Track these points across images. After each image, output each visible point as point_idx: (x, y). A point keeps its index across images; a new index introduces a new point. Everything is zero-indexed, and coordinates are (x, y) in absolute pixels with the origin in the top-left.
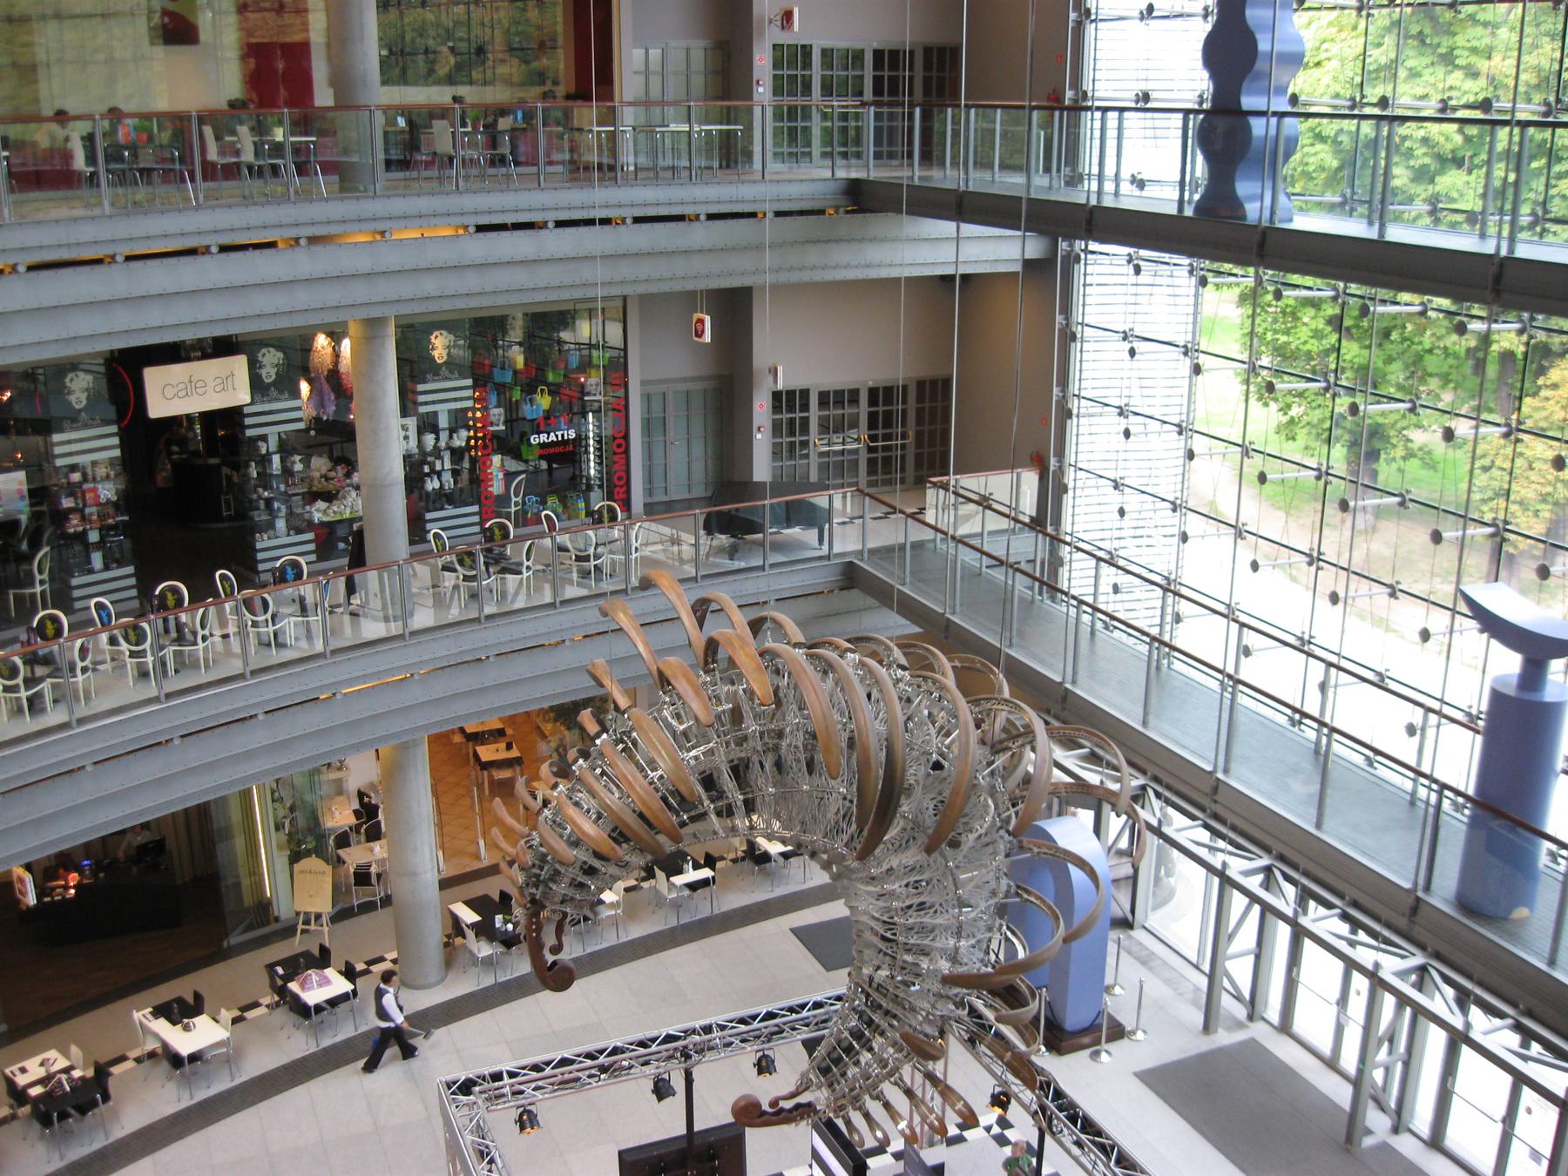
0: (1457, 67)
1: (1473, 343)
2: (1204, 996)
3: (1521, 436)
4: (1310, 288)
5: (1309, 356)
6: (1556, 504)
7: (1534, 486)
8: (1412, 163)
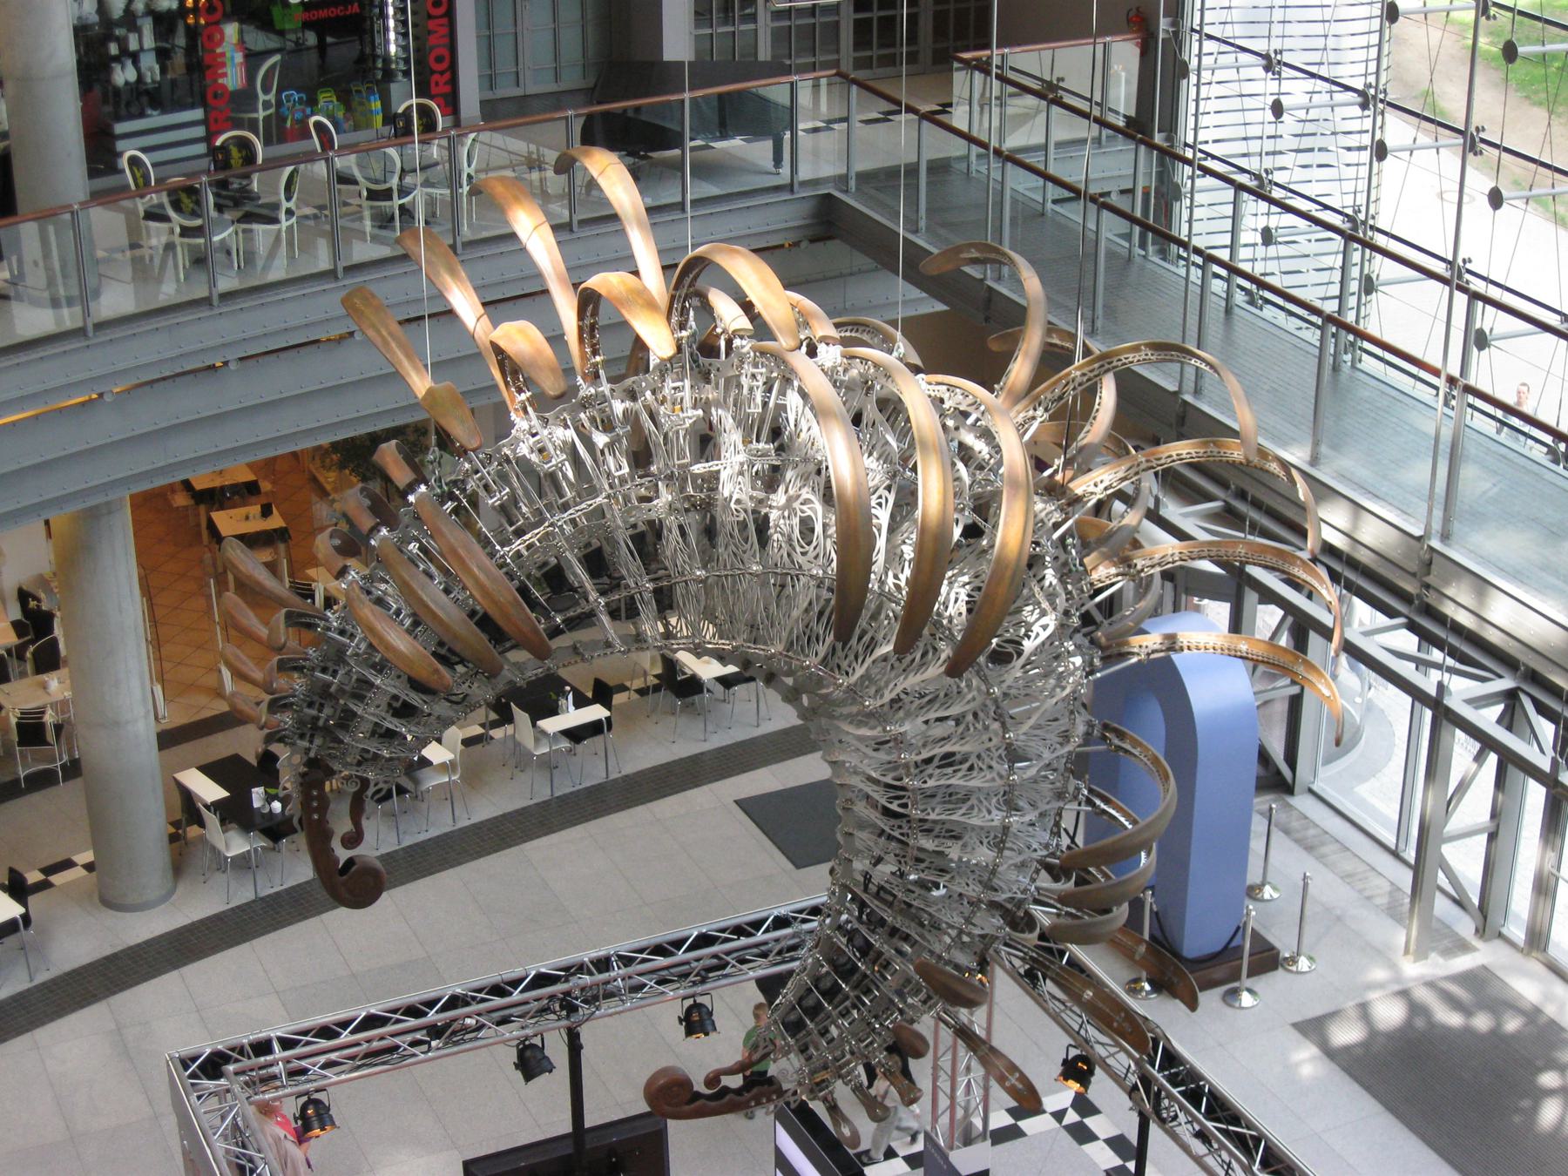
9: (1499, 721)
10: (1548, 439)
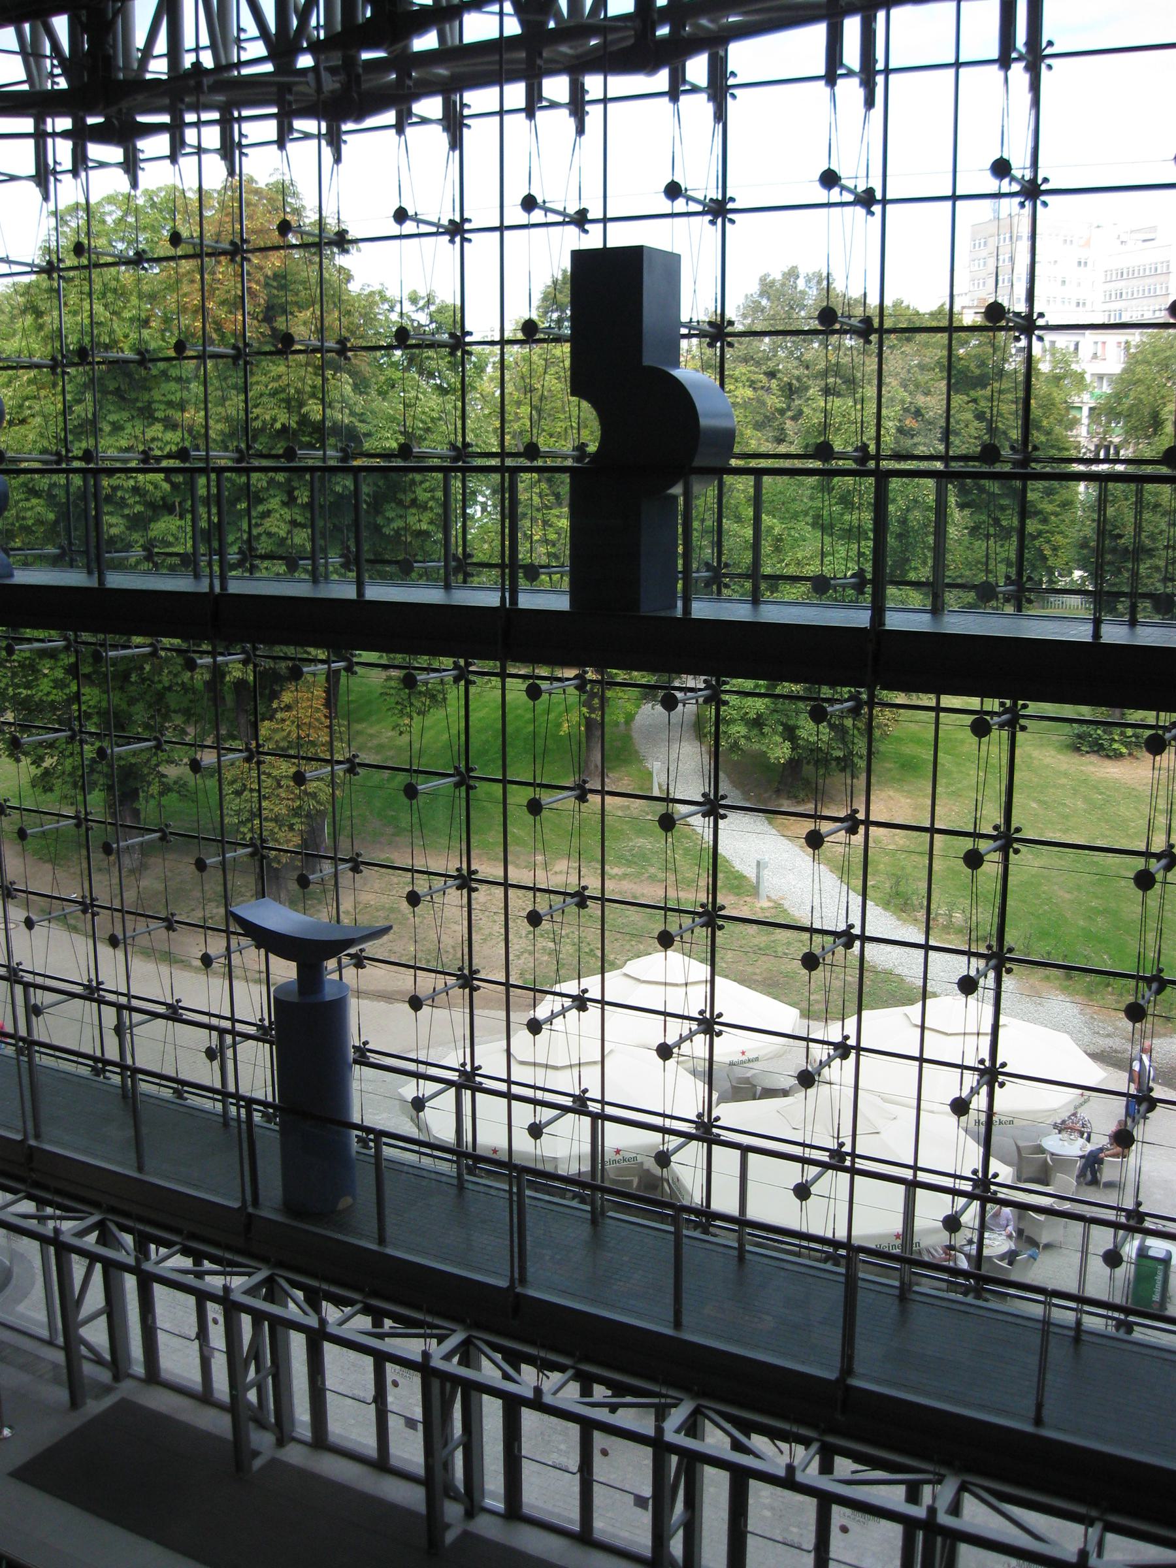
0: (158, 420)
1: (207, 677)
2: (65, 1371)
3: (262, 758)
4: (42, 641)
5: (53, 706)
6: (308, 816)
7: (285, 802)
8: (126, 512)
9: (97, 1242)
10: (91, 1063)
